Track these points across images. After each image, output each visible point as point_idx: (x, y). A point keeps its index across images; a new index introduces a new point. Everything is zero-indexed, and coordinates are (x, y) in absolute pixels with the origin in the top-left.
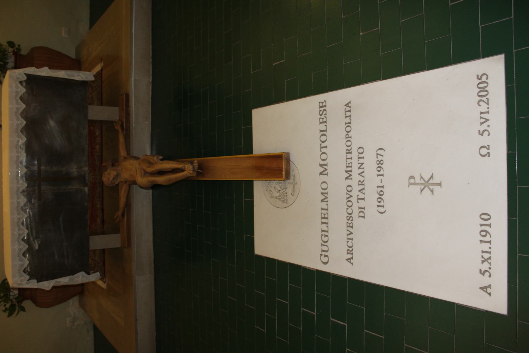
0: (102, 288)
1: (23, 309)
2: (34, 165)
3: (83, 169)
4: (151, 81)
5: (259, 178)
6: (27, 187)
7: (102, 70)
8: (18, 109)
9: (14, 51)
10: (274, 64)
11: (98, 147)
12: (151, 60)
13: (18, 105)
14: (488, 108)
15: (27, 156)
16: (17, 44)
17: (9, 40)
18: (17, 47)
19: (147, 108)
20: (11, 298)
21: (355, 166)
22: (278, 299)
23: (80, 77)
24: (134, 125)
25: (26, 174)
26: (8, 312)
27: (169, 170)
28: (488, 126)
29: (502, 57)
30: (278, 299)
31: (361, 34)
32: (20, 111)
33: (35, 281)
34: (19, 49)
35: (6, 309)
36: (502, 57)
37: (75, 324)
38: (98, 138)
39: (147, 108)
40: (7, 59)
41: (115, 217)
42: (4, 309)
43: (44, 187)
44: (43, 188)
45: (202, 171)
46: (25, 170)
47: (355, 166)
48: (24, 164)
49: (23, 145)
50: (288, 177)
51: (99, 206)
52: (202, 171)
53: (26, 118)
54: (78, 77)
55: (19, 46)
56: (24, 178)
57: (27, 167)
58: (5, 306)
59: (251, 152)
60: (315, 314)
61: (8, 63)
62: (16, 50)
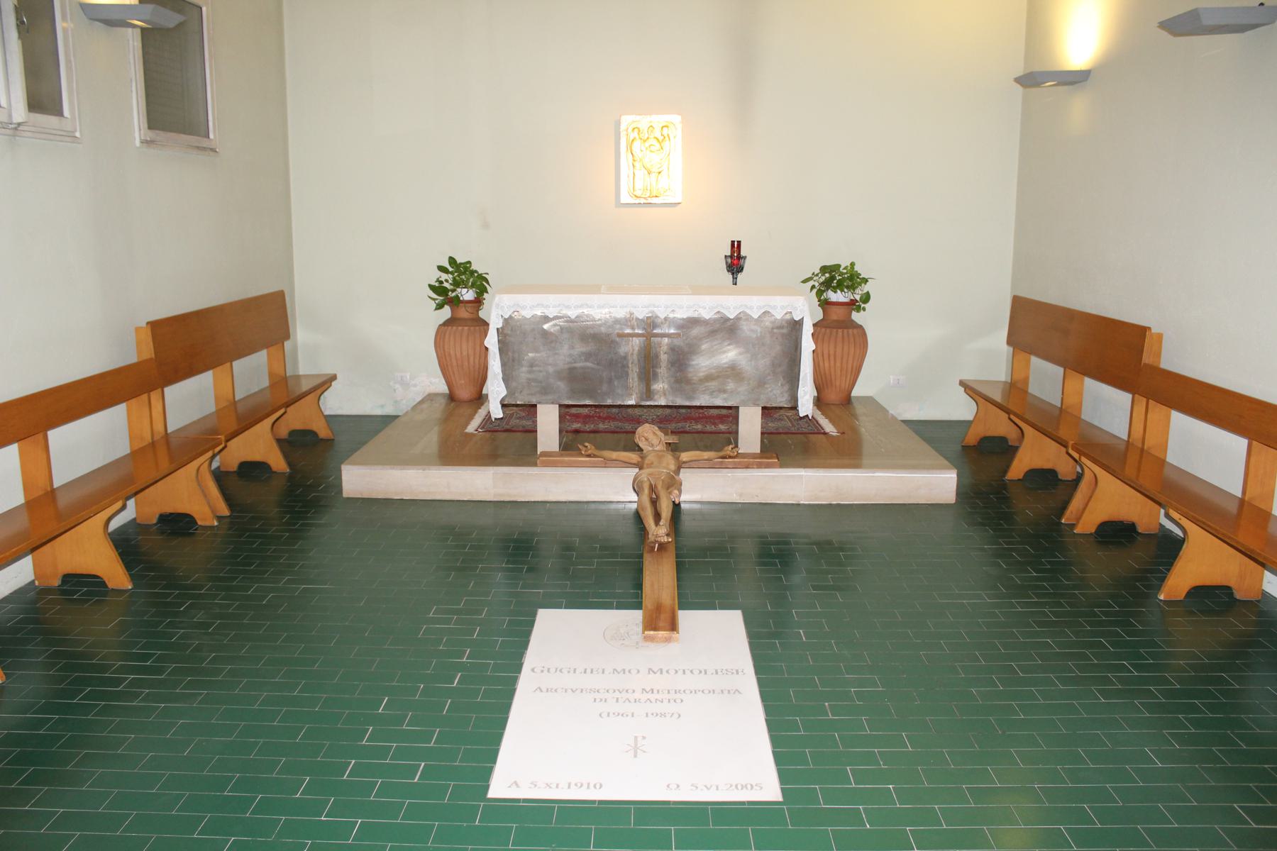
0: (467, 424)
1: (440, 307)
2: (669, 327)
3: (662, 398)
4: (802, 502)
5: (644, 617)
6: (637, 319)
7: (825, 433)
8: (751, 308)
9: (857, 301)
10: (801, 631)
11: (699, 427)
12: (835, 503)
13: (757, 308)
14: (722, 790)
15: (683, 319)
16: (866, 306)
17: (338, 376)
18: (863, 306)
19: (757, 496)
20: (459, 290)
21: (659, 697)
22: (468, 652)
23: (802, 395)
24: (729, 474)
25: (657, 317)
26: (437, 284)
27: (658, 509)
28: (702, 790)
29: (780, 799)
30: (468, 652)
31: (827, 704)
32: (748, 311)
33: (500, 326)
34: (858, 309)
35: (441, 282)
36: (780, 799)
37: (397, 386)
38: (713, 427)
39: (757, 496)
40: (841, 292)
41: (587, 444)
42: (443, 279)
43: (637, 341)
44: (636, 341)
45: (656, 550)
46: (662, 316)
47: (659, 697)
48: (671, 316)
49: (699, 314)
50: (647, 639)
51: (601, 426)
52: (656, 550)
53: (738, 318)
54: (802, 392)
55: (864, 309)
56: (650, 315)
57: (666, 319)
58: (447, 281)
59: (681, 608)
60: (464, 660)
61: (835, 292)
62: (857, 304)
